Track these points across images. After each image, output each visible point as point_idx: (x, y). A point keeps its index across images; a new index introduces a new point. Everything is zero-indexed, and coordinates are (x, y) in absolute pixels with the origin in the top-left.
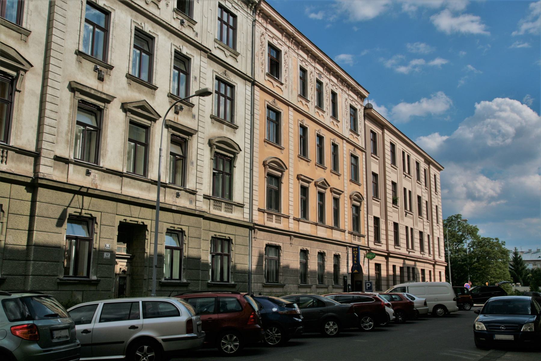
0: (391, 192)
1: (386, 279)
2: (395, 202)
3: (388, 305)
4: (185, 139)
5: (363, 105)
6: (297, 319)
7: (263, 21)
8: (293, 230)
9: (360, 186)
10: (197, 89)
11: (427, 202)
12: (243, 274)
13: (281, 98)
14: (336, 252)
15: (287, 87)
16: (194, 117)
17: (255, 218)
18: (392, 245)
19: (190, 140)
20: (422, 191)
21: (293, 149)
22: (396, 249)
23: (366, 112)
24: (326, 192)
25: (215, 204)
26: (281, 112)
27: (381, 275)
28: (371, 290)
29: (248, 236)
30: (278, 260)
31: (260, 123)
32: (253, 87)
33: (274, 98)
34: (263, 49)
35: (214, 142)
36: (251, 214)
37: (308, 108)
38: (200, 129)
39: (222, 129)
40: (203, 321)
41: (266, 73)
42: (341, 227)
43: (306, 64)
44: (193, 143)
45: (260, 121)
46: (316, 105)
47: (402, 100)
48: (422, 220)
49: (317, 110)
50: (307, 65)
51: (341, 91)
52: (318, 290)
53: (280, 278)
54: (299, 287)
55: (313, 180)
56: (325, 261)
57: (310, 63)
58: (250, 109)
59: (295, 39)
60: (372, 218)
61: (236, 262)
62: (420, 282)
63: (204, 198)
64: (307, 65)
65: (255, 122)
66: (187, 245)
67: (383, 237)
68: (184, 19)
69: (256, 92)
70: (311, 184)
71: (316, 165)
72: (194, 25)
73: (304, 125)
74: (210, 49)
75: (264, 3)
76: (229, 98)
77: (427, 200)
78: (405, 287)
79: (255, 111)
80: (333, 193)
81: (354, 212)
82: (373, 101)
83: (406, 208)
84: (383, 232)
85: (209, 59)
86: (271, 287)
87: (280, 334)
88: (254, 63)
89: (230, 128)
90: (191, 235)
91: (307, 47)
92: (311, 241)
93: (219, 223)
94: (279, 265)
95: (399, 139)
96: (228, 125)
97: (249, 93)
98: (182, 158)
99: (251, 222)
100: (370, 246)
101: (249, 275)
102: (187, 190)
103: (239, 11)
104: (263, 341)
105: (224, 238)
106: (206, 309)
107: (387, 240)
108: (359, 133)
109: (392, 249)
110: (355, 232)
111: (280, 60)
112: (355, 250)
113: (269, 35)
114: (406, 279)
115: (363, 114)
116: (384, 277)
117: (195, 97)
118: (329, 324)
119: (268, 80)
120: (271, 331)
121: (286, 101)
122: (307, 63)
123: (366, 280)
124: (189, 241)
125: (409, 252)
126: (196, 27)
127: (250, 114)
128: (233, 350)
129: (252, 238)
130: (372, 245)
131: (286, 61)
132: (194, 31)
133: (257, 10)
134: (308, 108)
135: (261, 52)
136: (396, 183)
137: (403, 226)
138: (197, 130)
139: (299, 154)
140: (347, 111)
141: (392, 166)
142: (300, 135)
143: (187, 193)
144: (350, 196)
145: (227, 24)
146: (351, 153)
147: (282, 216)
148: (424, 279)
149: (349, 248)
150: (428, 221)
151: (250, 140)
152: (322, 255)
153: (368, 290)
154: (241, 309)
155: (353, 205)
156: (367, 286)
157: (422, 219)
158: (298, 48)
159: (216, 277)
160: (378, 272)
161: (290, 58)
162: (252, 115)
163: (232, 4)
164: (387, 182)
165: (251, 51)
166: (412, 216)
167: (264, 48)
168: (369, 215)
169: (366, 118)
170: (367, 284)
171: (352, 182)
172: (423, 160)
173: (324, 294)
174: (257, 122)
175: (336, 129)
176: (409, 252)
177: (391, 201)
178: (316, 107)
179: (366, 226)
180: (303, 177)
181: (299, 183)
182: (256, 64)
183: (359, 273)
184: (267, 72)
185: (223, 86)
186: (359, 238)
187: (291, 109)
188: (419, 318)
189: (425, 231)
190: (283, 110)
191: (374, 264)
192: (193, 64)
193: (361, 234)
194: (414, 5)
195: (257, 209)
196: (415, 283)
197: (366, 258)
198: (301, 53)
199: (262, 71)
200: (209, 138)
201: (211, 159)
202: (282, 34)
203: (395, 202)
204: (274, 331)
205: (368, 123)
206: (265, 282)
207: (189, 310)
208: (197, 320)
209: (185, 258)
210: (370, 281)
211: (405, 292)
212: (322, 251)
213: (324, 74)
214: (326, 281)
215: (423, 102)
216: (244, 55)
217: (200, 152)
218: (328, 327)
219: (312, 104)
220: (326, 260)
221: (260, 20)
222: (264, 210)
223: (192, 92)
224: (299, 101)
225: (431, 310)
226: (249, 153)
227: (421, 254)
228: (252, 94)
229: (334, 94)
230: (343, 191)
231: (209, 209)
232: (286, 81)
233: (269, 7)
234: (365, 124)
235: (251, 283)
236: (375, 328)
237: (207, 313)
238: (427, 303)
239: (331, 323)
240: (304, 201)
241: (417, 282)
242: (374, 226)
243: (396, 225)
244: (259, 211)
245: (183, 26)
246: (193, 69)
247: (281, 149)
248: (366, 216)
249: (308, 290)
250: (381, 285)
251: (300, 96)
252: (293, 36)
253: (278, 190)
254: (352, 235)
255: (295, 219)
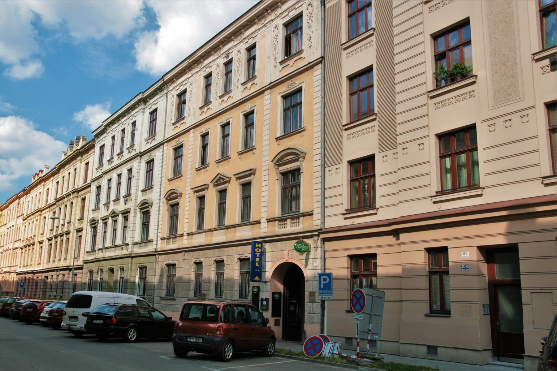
152: (220, 263)
153: (323, 289)
156: (323, 282)
170: (322, 277)
188: (34, 323)
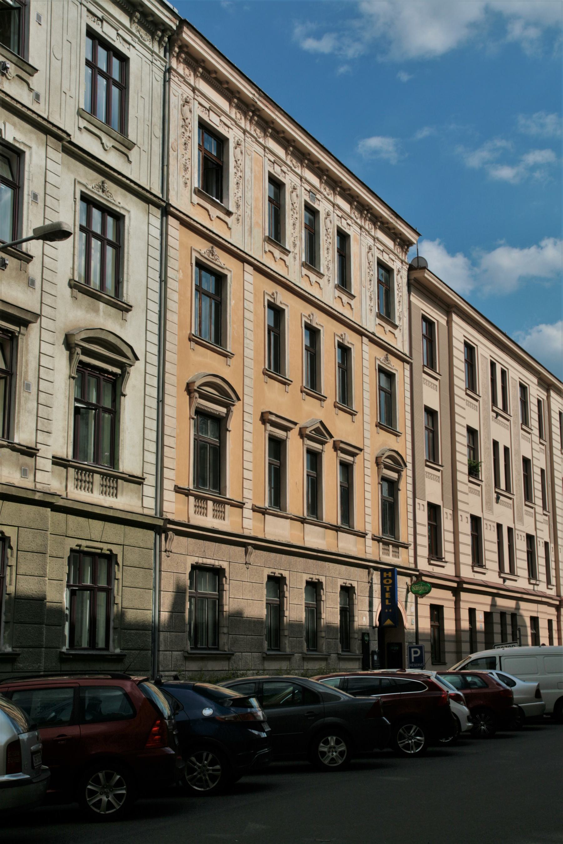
0: (465, 450)
1: (454, 639)
2: (474, 471)
3: (457, 698)
4: (12, 333)
5: (406, 261)
6: (256, 732)
7: (187, 71)
8: (252, 534)
9: (399, 436)
10: (38, 224)
11: (542, 471)
12: (141, 632)
13: (226, 244)
14: (345, 581)
15: (240, 221)
16: (31, 283)
17: (167, 507)
18: (468, 565)
19: (24, 335)
20: (532, 448)
21: (252, 357)
22: (476, 574)
23: (412, 277)
24: (325, 450)
25: (80, 478)
26: (226, 276)
27: (443, 629)
28: (421, 665)
29: (153, 546)
30: (219, 600)
31: (179, 299)
32: (164, 218)
33: (210, 245)
34: (188, 134)
35: (77, 340)
36: (159, 498)
37: (287, 267)
38: (46, 311)
39: (96, 311)
40: (45, 743)
41: (195, 188)
42: (358, 526)
43: (281, 170)
44: (29, 343)
45: (180, 295)
46: (304, 260)
47: (502, 242)
48: (532, 511)
49: (305, 271)
50: (285, 173)
51: (359, 230)
52: (305, 664)
53: (223, 639)
54: (263, 657)
55: (295, 424)
56: (321, 600)
57: (290, 167)
58: (158, 268)
59: (258, 113)
60: (423, 505)
61: (125, 605)
62: (530, 648)
63: (54, 463)
64: (285, 173)
65: (168, 295)
66: (14, 568)
67: (447, 547)
68: (7, 62)
69: (171, 231)
70: (290, 434)
71: (302, 392)
72: (31, 75)
73: (278, 303)
74: (68, 132)
75: (191, 31)
76: (110, 243)
77: (544, 468)
78: (495, 657)
79: (170, 273)
80: (339, 452)
81: (386, 494)
82: (439, 244)
83: (497, 484)
84: (447, 536)
85: (64, 155)
86: (203, 658)
87: (218, 767)
88: (168, 166)
89: (113, 310)
90: (23, 546)
91: (284, 131)
92: (291, 557)
93: (87, 519)
94: (221, 611)
95: (484, 336)
96: (108, 303)
97: (156, 233)
98: (4, 375)
99: (158, 516)
100: (419, 568)
101: (153, 634)
102: (17, 446)
103: (134, 47)
104: (180, 783)
105: (99, 551)
106: (53, 714)
107: (456, 553)
108: (397, 323)
109: (466, 572)
110: (387, 538)
111: (225, 159)
112: (388, 577)
113: (200, 104)
114: (497, 638)
115: (405, 280)
116: (450, 636)
117: (34, 241)
118: (327, 742)
119: (198, 204)
120: (200, 760)
121: (238, 251)
122: (284, 168)
123: (410, 640)
124: (19, 559)
125: (505, 580)
126: (36, 81)
127: (158, 280)
128: (113, 807)
129: (160, 551)
130: (423, 565)
131: (239, 162)
132: (31, 90)
133: (174, 46)
134: (287, 267)
135: (183, 140)
136: (477, 431)
137: (492, 524)
138: (39, 312)
139: (267, 367)
140: (371, 273)
141: (467, 394)
142: (269, 326)
143: (15, 453)
144: (377, 458)
145: (107, 76)
146: (379, 365)
147: (228, 504)
148: (536, 640)
149: (375, 572)
150: (545, 512)
151: (157, 337)
153: (414, 663)
154: (131, 712)
155: (384, 479)
156: (413, 656)
157: (532, 508)
158: (265, 134)
159: (81, 637)
160: (437, 624)
161: (247, 156)
162: (163, 280)
163: (117, 30)
164: (458, 428)
165: (161, 139)
166: (510, 502)
167: (190, 131)
168: (417, 501)
169: (412, 289)
171: (381, 428)
172: (535, 380)
173: (318, 674)
174: (173, 296)
175: (346, 312)
176: (505, 580)
177: (466, 469)
178: (304, 265)
179: (411, 523)
180: (273, 418)
181: (265, 430)
182: (171, 167)
183: (395, 627)
184: (196, 185)
185: (96, 214)
186: (396, 550)
187: (248, 268)
189: (539, 534)
190: (230, 271)
191: (429, 607)
192: (29, 165)
193: (401, 540)
194: (537, 24)
195: (172, 488)
196: (516, 649)
197: (410, 594)
198: (271, 144)
199: (186, 183)
200: (66, 331)
201: (71, 377)
202: (230, 101)
203: (474, 471)
204: (206, 760)
205: (416, 300)
206: (188, 648)
207: (13, 720)
208: (31, 741)
209: (10, 598)
210: (421, 643)
211: (494, 668)
212: (315, 578)
213: (322, 193)
214: (323, 644)
215: (546, 245)
216: (146, 147)
217: (44, 361)
218: (326, 750)
219: (295, 258)
220: (323, 598)
221: (181, 69)
222: (189, 490)
223: (27, 232)
224: (266, 252)
225: (550, 707)
226: (157, 364)
227: (530, 583)
228: (161, 235)
229: (343, 237)
230: (361, 447)
231: (64, 489)
232: (238, 206)
233: (201, 40)
234: (410, 302)
235: (159, 651)
236: (430, 749)
237: (56, 723)
238: (542, 691)
239: (332, 740)
240: (275, 469)
241: (520, 645)
242: (429, 524)
243: (476, 521)
244: (176, 492)
245: (4, 78)
246: (29, 176)
247: (226, 356)
248: (410, 501)
249: (284, 665)
250: (444, 652)
251: (268, 240)
252: (254, 106)
253: (219, 447)
254: (381, 544)
255: (256, 509)
